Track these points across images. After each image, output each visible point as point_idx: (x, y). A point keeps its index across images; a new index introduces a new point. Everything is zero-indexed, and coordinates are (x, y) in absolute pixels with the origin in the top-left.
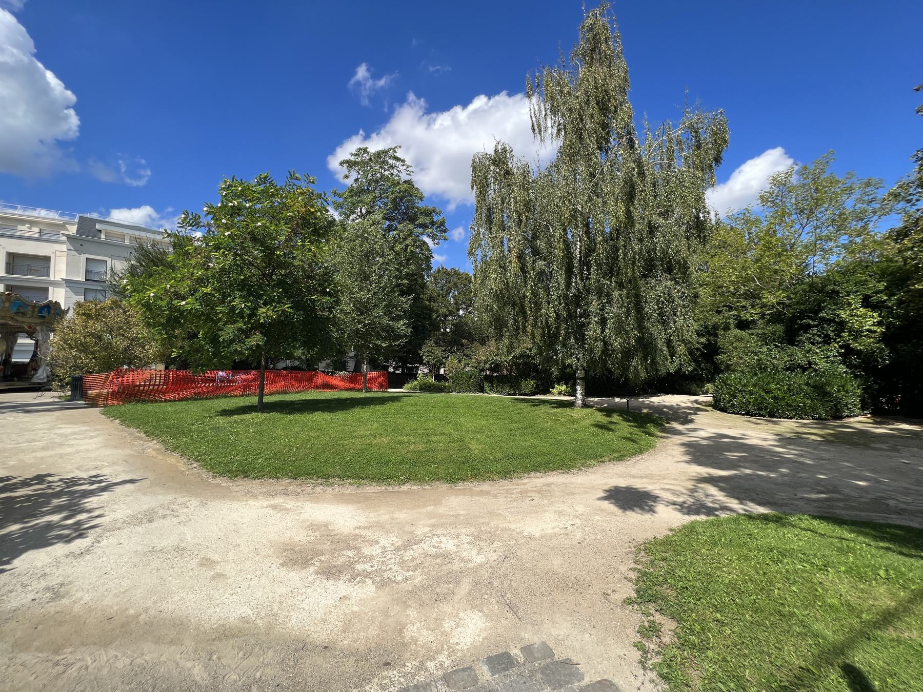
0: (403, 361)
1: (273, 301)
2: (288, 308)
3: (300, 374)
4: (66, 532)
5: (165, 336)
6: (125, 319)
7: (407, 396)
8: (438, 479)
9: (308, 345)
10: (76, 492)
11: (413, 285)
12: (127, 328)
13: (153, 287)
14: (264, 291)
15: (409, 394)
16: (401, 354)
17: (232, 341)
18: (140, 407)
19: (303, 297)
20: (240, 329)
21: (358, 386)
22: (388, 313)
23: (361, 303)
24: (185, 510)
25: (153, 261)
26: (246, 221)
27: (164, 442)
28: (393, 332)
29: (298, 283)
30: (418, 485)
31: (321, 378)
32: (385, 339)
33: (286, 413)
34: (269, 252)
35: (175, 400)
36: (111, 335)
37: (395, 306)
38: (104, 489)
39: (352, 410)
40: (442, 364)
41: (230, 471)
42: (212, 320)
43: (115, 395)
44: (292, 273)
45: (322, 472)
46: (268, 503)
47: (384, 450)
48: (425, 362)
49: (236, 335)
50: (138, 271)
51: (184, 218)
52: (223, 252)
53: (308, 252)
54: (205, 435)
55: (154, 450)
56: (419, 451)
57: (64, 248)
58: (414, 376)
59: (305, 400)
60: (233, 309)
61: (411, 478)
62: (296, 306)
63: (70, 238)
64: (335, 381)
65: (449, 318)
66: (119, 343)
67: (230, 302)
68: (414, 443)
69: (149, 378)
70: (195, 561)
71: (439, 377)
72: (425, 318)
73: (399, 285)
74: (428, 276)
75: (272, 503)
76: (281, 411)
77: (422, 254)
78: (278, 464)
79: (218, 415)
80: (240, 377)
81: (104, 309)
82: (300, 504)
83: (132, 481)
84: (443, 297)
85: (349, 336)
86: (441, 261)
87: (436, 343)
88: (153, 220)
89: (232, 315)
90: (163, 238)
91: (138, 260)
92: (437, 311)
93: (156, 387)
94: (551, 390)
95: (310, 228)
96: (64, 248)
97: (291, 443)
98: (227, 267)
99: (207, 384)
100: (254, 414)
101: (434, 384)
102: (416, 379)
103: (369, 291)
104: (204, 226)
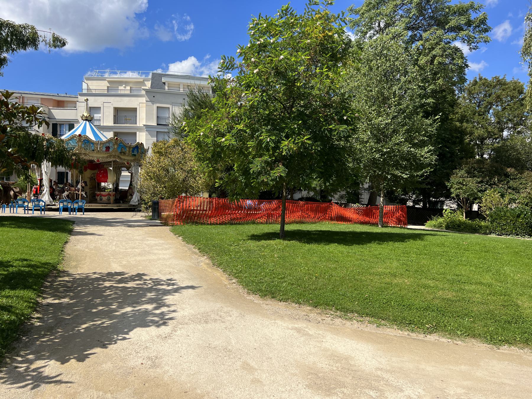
0: (425, 194)
1: (294, 133)
2: (307, 139)
3: (315, 205)
4: (156, 319)
5: (211, 169)
6: (182, 155)
7: (427, 234)
8: (474, 336)
9: (325, 176)
10: (160, 290)
11: (439, 104)
12: (184, 162)
13: (202, 126)
14: (286, 124)
15: (433, 233)
16: (424, 186)
17: (259, 173)
18: (194, 227)
19: (321, 128)
20: (266, 162)
21: (373, 220)
22: (409, 140)
23: (379, 130)
24: (229, 318)
25: (199, 104)
26: (270, 56)
27: (212, 258)
28: (415, 161)
29: (316, 114)
30: (448, 338)
31: (336, 210)
32: (405, 168)
33: (304, 243)
34: (290, 84)
35: (217, 224)
36: (174, 168)
37: (418, 131)
38: (176, 290)
39: (369, 245)
40: (477, 198)
41: (260, 290)
42: (244, 154)
43: (179, 217)
44: (310, 103)
45: (341, 305)
46: (292, 325)
47: (406, 292)
48: (453, 195)
49: (263, 168)
50: (190, 114)
51: (223, 63)
52: (253, 90)
53: (326, 79)
54: (241, 255)
55: (205, 264)
56: (448, 300)
57: (143, 100)
58: (439, 213)
59: (321, 231)
60: (261, 142)
61: (436, 328)
62: (315, 138)
63: (147, 91)
64: (349, 213)
65: (488, 141)
66: (180, 175)
67: (258, 137)
68: (442, 289)
69: (199, 204)
70: (239, 363)
71: (471, 215)
72: (454, 143)
73: (422, 106)
74: (461, 90)
75: (296, 326)
76: (300, 240)
77: (454, 65)
78: (300, 290)
79: (249, 239)
80: (264, 206)
81: (169, 147)
82: (321, 332)
83: (192, 287)
84: (479, 115)
85: (365, 166)
86: (477, 70)
87: (468, 172)
88: (197, 68)
89: (260, 148)
90: (208, 84)
91: (190, 105)
92: (471, 134)
93: (204, 212)
94: (103, 184)
95: (328, 53)
96: (143, 100)
97: (311, 272)
98: (256, 104)
99: (240, 211)
100: (277, 241)
101: (464, 223)
102: (442, 216)
103: (388, 114)
104: (237, 67)
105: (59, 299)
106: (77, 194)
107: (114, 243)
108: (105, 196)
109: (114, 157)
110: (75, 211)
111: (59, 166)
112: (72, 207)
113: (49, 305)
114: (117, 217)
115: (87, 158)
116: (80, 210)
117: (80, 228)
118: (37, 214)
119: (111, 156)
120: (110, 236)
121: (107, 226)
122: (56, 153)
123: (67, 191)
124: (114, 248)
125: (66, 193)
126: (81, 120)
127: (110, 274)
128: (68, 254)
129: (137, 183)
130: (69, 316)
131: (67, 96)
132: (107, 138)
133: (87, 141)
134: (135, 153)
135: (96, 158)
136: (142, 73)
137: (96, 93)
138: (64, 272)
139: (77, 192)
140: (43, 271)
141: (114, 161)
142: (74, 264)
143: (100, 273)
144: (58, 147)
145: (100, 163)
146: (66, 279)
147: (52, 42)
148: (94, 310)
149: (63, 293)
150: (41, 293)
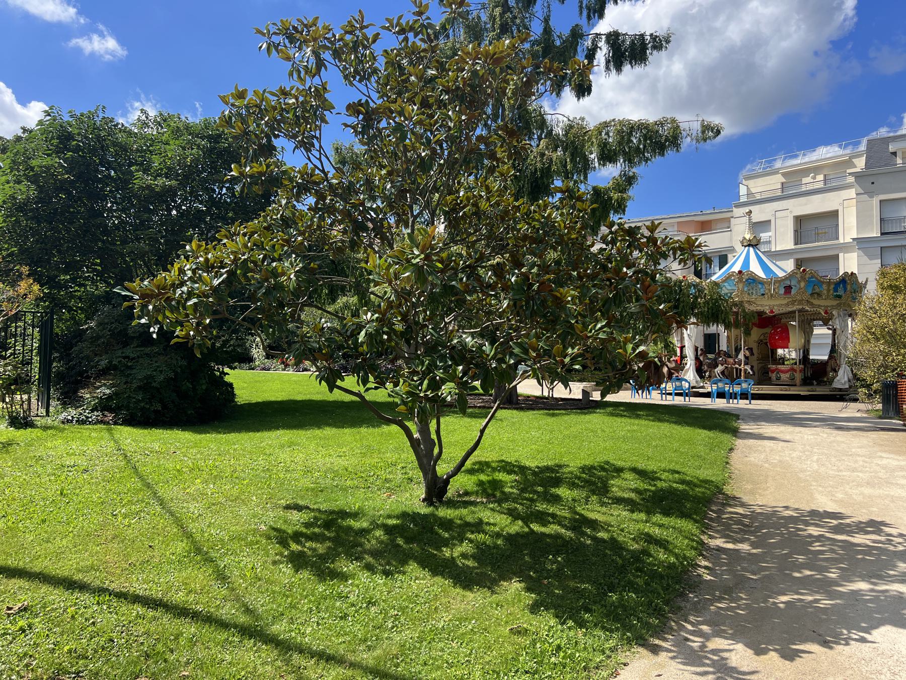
94: (780, 352)
105: (734, 543)
106: (737, 369)
107: (815, 458)
108: (783, 372)
109: (800, 302)
110: (736, 398)
111: (713, 325)
112: (731, 391)
113: (719, 549)
114: (811, 411)
115: (753, 308)
116: (744, 396)
117: (750, 427)
118: (679, 401)
119: (795, 301)
120: (805, 445)
121: (795, 425)
122: (709, 304)
123: (722, 365)
124: (815, 466)
125: (720, 368)
126: (739, 248)
127: (814, 513)
128: (736, 469)
129: (845, 347)
130: (755, 574)
131: (716, 211)
132: (786, 272)
133: (753, 280)
134: (840, 292)
135: (767, 308)
136: (846, 146)
137: (763, 197)
138: (734, 498)
139: (737, 366)
140: (703, 493)
141: (800, 311)
142: (749, 487)
143: (797, 509)
144: (711, 295)
145: (774, 316)
146: (740, 510)
147: (700, 135)
148: (797, 575)
149: (738, 533)
150: (705, 528)
